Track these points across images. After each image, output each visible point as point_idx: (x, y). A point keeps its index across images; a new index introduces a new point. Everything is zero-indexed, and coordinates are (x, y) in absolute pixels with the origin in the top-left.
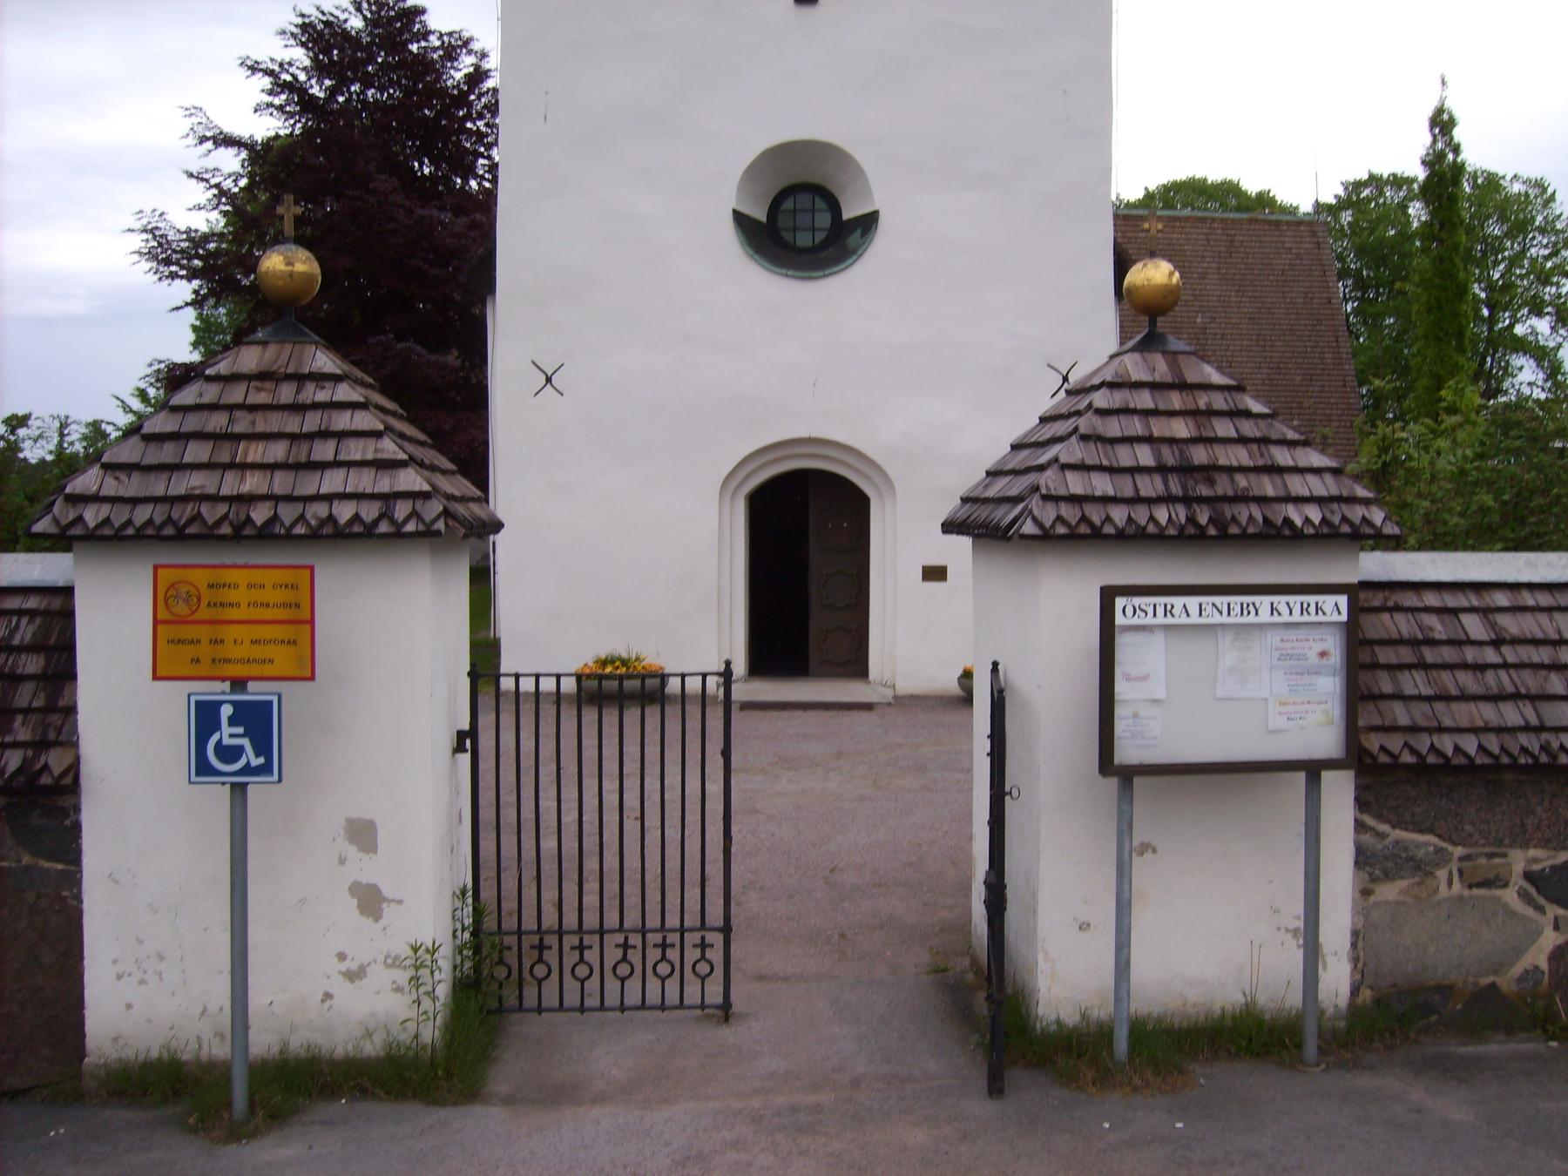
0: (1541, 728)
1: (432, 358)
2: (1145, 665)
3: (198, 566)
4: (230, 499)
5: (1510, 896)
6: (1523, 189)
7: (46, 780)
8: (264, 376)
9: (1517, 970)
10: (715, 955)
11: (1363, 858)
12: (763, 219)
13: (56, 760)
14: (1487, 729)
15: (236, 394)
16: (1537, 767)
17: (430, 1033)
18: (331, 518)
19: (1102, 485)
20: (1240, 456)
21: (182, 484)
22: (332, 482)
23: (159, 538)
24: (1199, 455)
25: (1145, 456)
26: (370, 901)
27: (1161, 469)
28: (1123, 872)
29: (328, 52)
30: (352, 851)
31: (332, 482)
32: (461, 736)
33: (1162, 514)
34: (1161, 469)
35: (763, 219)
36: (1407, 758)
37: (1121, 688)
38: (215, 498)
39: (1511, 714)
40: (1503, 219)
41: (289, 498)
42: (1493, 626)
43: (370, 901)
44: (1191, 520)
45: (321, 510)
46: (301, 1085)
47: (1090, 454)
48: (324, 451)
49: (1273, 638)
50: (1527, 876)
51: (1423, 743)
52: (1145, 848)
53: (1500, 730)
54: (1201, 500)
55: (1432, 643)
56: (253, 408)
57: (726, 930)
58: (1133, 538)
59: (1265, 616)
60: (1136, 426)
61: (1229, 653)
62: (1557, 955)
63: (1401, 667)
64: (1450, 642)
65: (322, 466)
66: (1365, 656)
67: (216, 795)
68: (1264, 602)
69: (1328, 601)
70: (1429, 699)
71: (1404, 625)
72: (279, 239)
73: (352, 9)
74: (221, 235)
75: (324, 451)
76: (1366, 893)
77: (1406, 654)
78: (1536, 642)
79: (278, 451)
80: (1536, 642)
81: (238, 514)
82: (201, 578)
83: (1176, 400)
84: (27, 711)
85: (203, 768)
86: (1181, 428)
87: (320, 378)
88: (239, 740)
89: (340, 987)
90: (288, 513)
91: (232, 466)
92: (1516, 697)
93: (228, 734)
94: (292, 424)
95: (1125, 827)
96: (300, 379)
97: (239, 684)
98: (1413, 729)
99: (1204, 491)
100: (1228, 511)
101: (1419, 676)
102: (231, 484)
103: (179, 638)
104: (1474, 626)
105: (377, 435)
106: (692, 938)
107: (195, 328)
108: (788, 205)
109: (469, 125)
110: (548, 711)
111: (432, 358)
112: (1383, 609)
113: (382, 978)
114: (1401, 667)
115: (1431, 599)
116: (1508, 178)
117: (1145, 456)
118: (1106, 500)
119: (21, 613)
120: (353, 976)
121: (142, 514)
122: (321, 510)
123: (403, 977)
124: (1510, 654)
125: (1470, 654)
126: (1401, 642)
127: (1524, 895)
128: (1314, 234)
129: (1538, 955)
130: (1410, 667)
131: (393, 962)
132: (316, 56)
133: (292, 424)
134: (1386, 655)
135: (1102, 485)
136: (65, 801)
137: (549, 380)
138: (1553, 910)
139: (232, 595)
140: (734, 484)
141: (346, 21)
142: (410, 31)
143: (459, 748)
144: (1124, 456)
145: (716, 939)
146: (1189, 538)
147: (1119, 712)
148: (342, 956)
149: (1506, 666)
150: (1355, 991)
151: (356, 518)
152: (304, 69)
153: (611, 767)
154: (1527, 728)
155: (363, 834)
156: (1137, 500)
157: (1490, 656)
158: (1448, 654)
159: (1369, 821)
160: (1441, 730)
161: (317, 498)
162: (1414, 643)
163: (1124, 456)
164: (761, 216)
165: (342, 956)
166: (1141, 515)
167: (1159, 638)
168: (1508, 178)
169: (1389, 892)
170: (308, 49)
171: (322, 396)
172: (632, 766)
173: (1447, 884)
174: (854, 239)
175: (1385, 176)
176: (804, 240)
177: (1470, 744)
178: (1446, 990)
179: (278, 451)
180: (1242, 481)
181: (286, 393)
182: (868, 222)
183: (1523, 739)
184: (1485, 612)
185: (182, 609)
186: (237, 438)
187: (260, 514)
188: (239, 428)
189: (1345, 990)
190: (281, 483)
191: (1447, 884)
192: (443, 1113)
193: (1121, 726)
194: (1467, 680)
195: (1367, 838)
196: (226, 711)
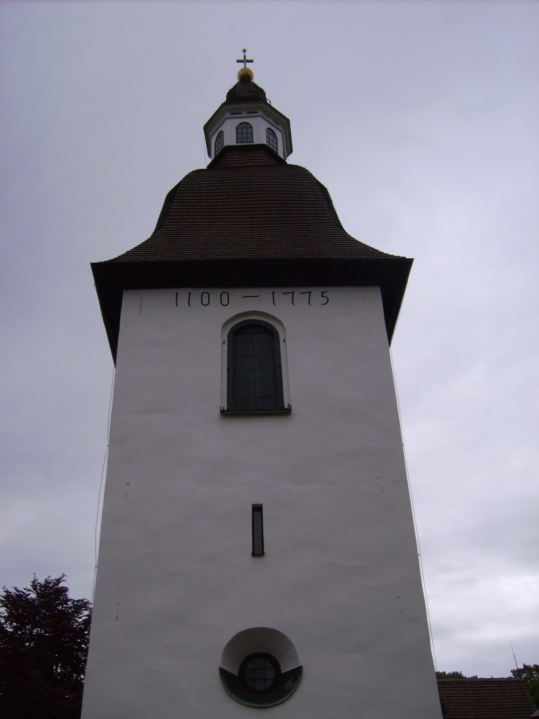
12: (236, 673)
29: (17, 611)
35: (236, 673)
73: (32, 589)
109: (83, 646)
132: (11, 611)
141: (29, 595)
142: (59, 599)
152: (5, 617)
164: (234, 671)
170: (8, 608)
175: (532, 666)
176: (260, 686)
182: (297, 673)
192: (239, 667)
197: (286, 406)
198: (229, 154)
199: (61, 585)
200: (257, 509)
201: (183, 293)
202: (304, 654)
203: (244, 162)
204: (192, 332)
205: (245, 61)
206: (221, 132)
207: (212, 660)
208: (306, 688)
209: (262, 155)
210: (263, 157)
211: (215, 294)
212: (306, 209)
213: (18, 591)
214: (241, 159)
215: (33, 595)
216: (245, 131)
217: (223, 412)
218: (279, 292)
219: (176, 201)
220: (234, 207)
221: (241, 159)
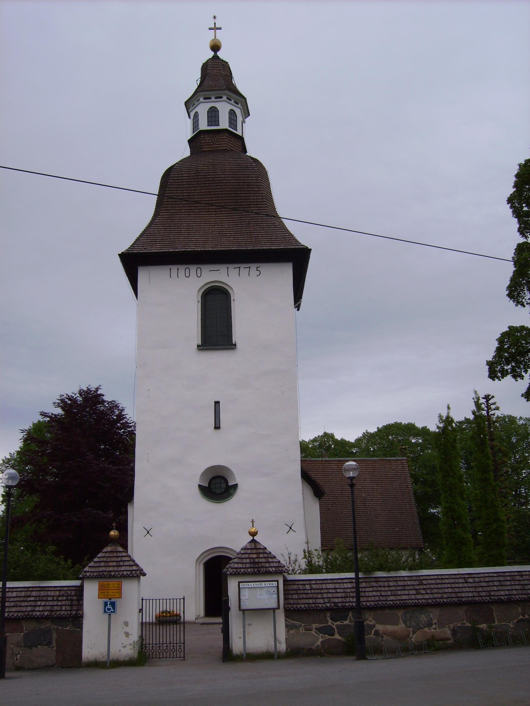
0: (315, 603)
1: (105, 515)
2: (245, 594)
3: (105, 581)
4: (108, 571)
5: (313, 632)
6: (524, 422)
7: (79, 615)
8: (111, 552)
9: (315, 645)
10: (182, 648)
11: (287, 626)
13: (80, 612)
14: (306, 604)
15: (107, 555)
16: (314, 610)
17: (136, 656)
18: (123, 574)
19: (240, 566)
20: (263, 560)
21: (101, 569)
22: (123, 568)
23: (98, 577)
24: (257, 560)
25: (248, 561)
26: (127, 634)
27: (250, 563)
28: (244, 627)
30: (124, 627)
31: (123, 568)
32: (140, 610)
33: (249, 570)
34: (250, 563)
36: (292, 608)
37: (241, 597)
38: (106, 571)
39: (311, 601)
40: (517, 435)
41: (117, 571)
42: (311, 587)
43: (127, 634)
44: (254, 571)
45: (121, 573)
46: (118, 664)
47: (239, 561)
48: (122, 564)
49: (266, 589)
50: (316, 629)
51: (295, 606)
52: (249, 625)
53: (308, 604)
54: (256, 567)
55: (300, 590)
56: (110, 557)
57: (184, 643)
58: (245, 574)
59: (264, 585)
60: (247, 556)
61: (259, 591)
62: (322, 642)
63: (294, 594)
64: (302, 590)
65: (121, 566)
66: (287, 592)
67: (107, 616)
68: (263, 583)
69: (274, 583)
70: (297, 599)
71: (295, 587)
72: (112, 529)
74: (15, 460)
75: (122, 564)
76: (288, 632)
77: (295, 592)
78: (318, 589)
79: (114, 564)
80: (318, 589)
81: (109, 573)
82: (106, 583)
83: (254, 551)
84: (75, 605)
85: (105, 612)
86: (255, 556)
87: (120, 552)
88: (110, 607)
89: (122, 649)
90: (117, 573)
91: (108, 566)
92: (312, 598)
93: (109, 606)
94: (116, 559)
95: (244, 619)
96: (117, 552)
97: (110, 599)
98: (294, 604)
99: (257, 566)
100: (260, 569)
101: (296, 595)
102: (108, 569)
103: (102, 592)
104: (308, 587)
105: (129, 561)
106: (178, 645)
107: (3, 496)
108: (214, 482)
110: (148, 626)
111: (105, 515)
112: (292, 584)
113: (128, 647)
114: (294, 594)
115: (301, 583)
116: (518, 418)
117: (248, 561)
118: (241, 568)
119: (72, 590)
120: (124, 647)
121: (95, 574)
122: (121, 573)
123: (132, 647)
124: (313, 591)
125: (306, 592)
126: (294, 590)
127: (315, 632)
128: (402, 464)
129: (319, 643)
130: (295, 594)
131: (130, 645)
133: (116, 559)
134: (291, 592)
135: (240, 566)
136: (81, 619)
137: (148, 532)
138: (321, 635)
139: (110, 586)
140: (200, 559)
143: (140, 612)
144: (245, 561)
145: (182, 645)
146: (253, 574)
147: (241, 601)
148: (122, 644)
149: (312, 593)
150: (287, 649)
151: (127, 574)
153: (165, 635)
154: (313, 603)
155: (126, 624)
156: (246, 568)
157: (309, 592)
158: (302, 592)
159: (287, 619)
160: (298, 604)
161: (121, 571)
162: (296, 590)
163: (245, 561)
165: (122, 644)
166: (246, 570)
167: (247, 589)
168: (518, 418)
169: (292, 632)
171: (121, 555)
172: (168, 636)
173: (302, 630)
174: (232, 491)
176: (218, 491)
177: (303, 606)
178: (303, 649)
179: (114, 564)
180: (263, 564)
181: (115, 554)
182: (235, 486)
183: (312, 605)
184: (310, 584)
185: (102, 588)
186: (108, 562)
187: (113, 574)
188: (109, 560)
189: (285, 649)
190: (115, 569)
191: (302, 630)
193: (242, 604)
194: (304, 596)
195: (287, 623)
196: (109, 603)
197: (234, 343)
198: (202, 136)
199: (99, 392)
200: (217, 403)
201: (174, 268)
202: (238, 478)
203: (212, 143)
204: (178, 293)
205: (215, 28)
206: (197, 112)
207: (195, 480)
208: (239, 494)
209: (225, 137)
210: (226, 140)
211: (193, 268)
212: (251, 198)
213: (69, 396)
214: (211, 141)
215: (80, 399)
216: (213, 113)
217: (198, 346)
218: (231, 267)
219: (167, 192)
220: (205, 196)
221: (211, 141)
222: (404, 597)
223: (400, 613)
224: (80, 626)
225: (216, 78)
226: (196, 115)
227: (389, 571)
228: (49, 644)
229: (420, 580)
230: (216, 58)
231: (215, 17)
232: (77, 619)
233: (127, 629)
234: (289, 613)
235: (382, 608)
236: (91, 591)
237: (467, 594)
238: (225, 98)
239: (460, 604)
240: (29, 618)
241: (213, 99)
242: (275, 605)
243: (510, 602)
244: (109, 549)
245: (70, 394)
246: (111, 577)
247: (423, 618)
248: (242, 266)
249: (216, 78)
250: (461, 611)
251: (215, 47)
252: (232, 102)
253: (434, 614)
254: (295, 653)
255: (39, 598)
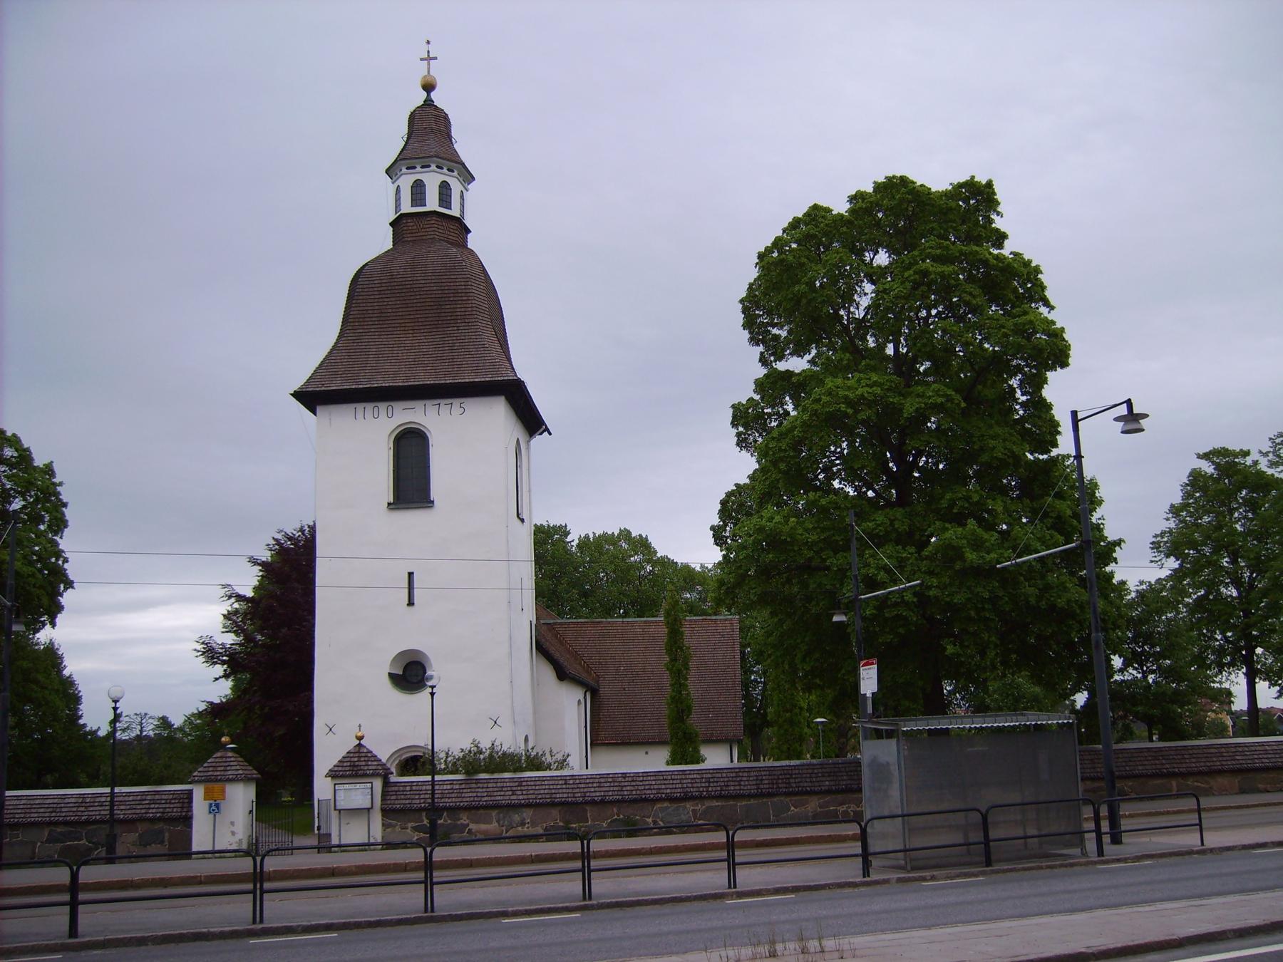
3: (210, 785)
26: (233, 833)
43: (233, 833)
58: (343, 777)
103: (208, 795)
155: (232, 823)
200: (411, 574)
201: (360, 406)
204: (368, 435)
205: (429, 59)
211: (383, 406)
218: (429, 403)
222: (499, 797)
223: (494, 813)
224: (190, 826)
225: (429, 134)
226: (398, 191)
227: (493, 772)
228: (162, 842)
229: (520, 782)
230: (428, 103)
231: (428, 42)
232: (187, 820)
233: (233, 829)
234: (385, 812)
235: (477, 808)
236: (198, 792)
237: (561, 796)
238: (433, 167)
239: (553, 804)
240: (142, 820)
241: (418, 169)
242: (369, 806)
243: (603, 802)
244: (219, 754)
245: (289, 531)
246: (217, 781)
247: (517, 818)
248: (443, 402)
249: (429, 134)
250: (555, 812)
251: (429, 87)
252: (445, 170)
253: (528, 814)
254: (388, 845)
255: (153, 802)
